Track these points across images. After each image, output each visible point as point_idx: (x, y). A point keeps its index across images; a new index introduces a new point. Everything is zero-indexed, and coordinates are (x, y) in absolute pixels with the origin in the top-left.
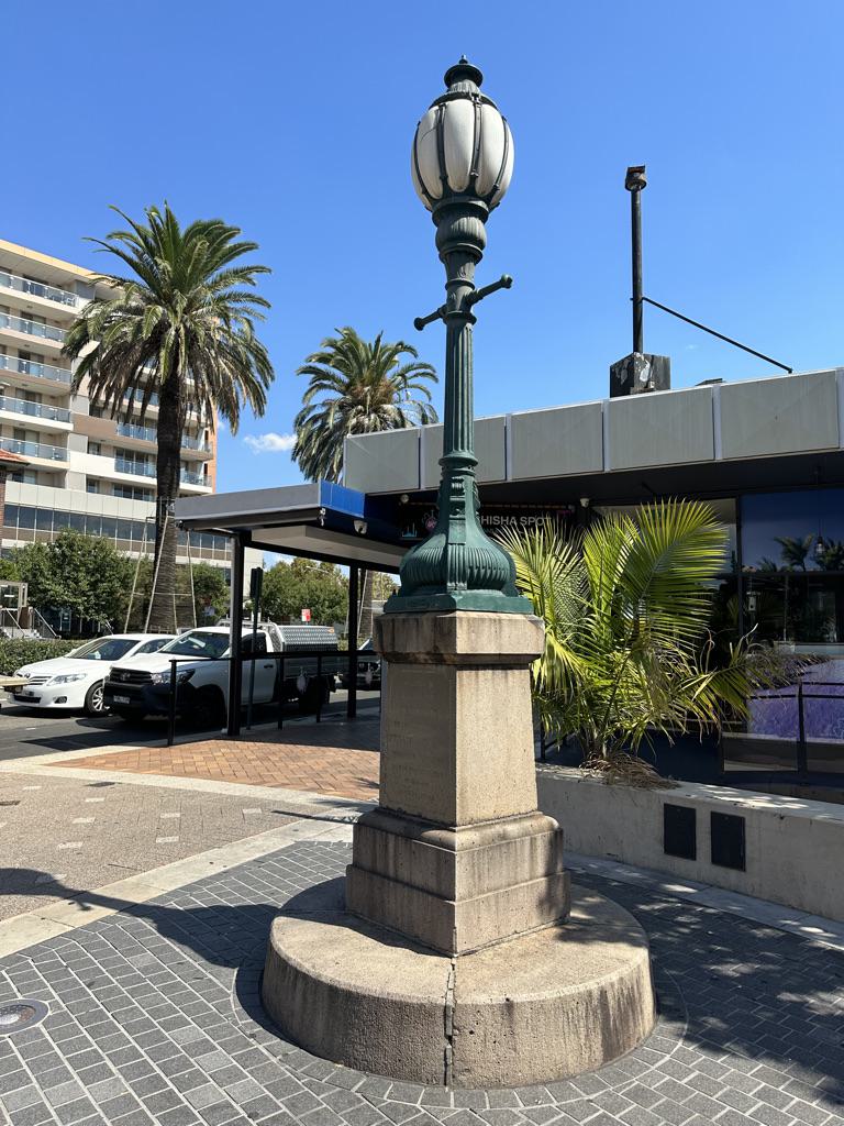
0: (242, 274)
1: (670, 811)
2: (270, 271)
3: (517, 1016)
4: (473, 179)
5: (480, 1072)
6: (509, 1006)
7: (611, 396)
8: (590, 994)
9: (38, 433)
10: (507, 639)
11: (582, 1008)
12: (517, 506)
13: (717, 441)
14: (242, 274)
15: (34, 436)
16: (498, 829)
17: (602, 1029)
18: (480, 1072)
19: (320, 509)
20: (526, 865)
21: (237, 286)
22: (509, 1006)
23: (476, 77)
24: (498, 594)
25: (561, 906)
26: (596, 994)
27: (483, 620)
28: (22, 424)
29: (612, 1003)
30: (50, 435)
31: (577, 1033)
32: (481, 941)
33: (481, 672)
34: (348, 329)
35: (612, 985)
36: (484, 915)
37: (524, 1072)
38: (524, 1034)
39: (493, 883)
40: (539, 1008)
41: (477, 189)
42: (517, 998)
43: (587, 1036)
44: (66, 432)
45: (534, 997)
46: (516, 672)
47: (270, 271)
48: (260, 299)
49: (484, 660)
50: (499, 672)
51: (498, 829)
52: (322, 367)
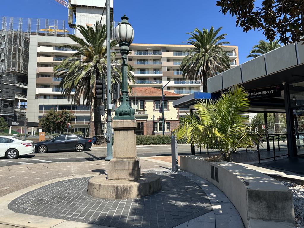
0: (220, 38)
1: (212, 168)
2: (227, 34)
3: (101, 186)
4: (120, 39)
5: (96, 195)
6: (100, 185)
7: (52, 91)
8: (114, 186)
9: (194, 88)
10: (125, 125)
11: (112, 188)
12: (261, 88)
13: (298, 56)
14: (220, 38)
15: (193, 88)
16: (122, 159)
17: (116, 193)
18: (96, 195)
19: (195, 99)
20: (127, 167)
21: (219, 41)
22: (100, 185)
23: (127, 19)
24: (129, 116)
25: (136, 176)
26: (116, 187)
27: (118, 121)
28: (190, 86)
29: (119, 189)
30: (197, 87)
31: (110, 192)
32: (114, 178)
33: (120, 131)
34: (261, 41)
35: (120, 186)
36: (115, 173)
37: (101, 196)
38: (102, 191)
39: (118, 169)
40: (104, 186)
41: (127, 41)
42: (101, 184)
43: (112, 193)
44: (200, 86)
45: (104, 184)
46: (117, 131)
47: (227, 34)
48: (227, 42)
49: (118, 129)
50: (125, 131)
51: (122, 159)
52: (254, 54)
